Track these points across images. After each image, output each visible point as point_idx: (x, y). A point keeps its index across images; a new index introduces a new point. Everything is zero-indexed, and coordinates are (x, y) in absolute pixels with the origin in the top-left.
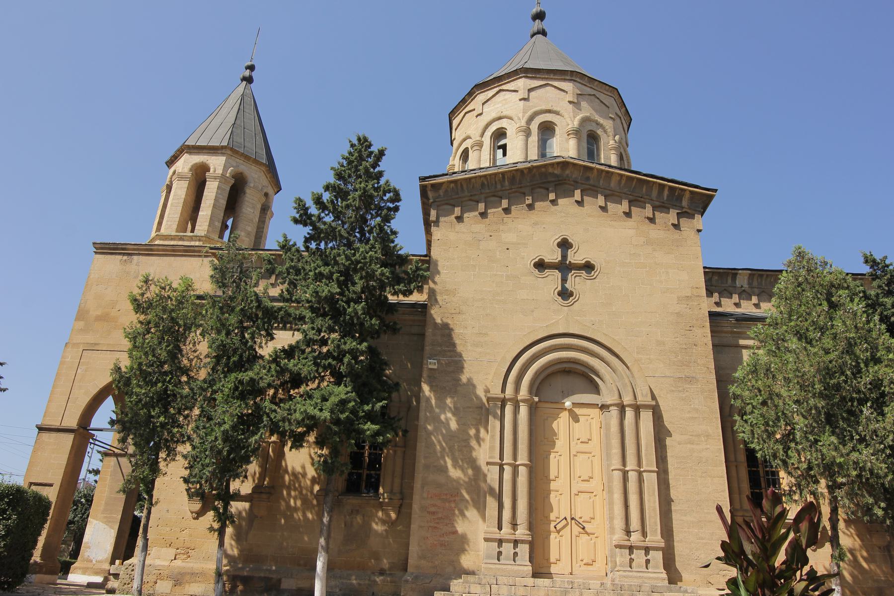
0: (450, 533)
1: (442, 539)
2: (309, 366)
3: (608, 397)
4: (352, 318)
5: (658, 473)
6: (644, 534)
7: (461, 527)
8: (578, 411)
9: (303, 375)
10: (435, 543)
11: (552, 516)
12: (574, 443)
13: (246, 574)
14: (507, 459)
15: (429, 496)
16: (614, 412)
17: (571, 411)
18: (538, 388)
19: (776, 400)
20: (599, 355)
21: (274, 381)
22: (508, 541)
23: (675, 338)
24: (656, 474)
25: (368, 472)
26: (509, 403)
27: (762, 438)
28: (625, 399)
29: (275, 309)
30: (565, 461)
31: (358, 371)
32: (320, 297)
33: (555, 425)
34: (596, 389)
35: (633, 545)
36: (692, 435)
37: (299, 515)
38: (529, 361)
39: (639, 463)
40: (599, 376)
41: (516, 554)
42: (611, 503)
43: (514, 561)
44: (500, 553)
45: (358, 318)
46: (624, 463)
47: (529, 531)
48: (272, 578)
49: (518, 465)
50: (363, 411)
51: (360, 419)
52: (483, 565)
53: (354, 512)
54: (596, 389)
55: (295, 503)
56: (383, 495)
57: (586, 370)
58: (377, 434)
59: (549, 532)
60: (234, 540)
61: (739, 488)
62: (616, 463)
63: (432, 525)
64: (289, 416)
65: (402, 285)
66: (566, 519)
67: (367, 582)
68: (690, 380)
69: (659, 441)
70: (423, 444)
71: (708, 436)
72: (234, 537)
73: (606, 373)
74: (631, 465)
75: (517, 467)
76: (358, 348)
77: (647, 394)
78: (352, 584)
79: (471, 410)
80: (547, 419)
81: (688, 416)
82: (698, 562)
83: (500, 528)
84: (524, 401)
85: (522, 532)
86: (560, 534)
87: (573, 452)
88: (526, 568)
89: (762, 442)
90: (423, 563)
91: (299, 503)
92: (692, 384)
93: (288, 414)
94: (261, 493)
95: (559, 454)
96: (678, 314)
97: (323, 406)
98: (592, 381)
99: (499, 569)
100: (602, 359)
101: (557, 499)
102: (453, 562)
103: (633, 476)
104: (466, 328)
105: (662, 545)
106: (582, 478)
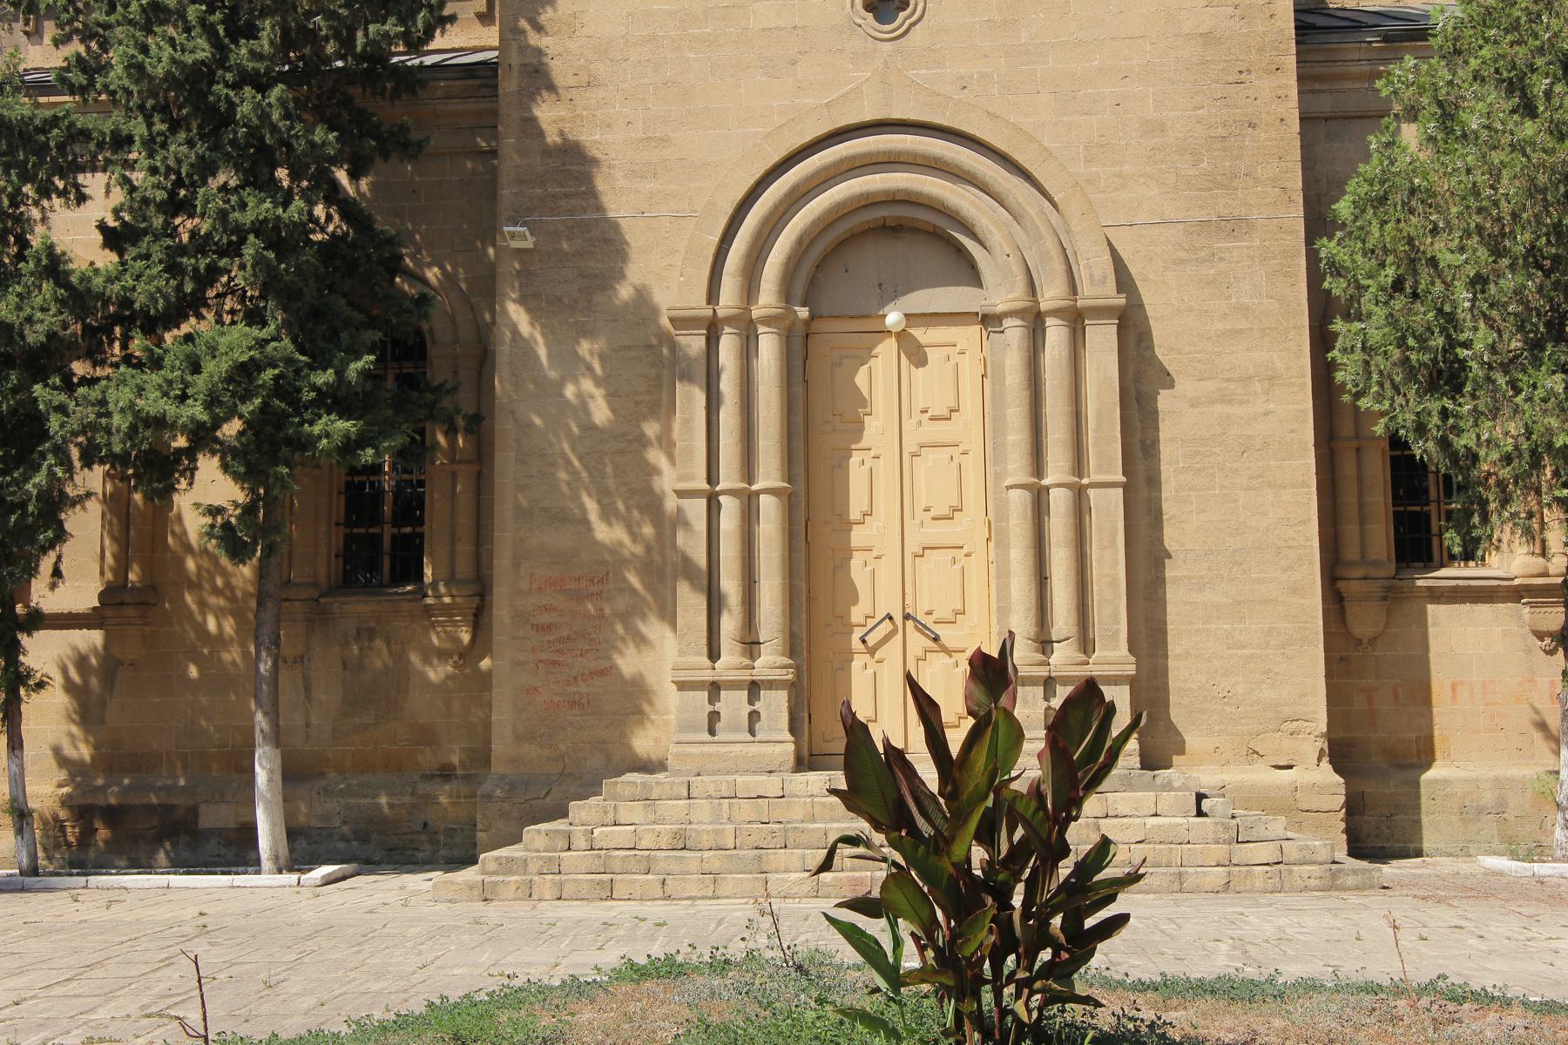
0: (591, 673)
1: (573, 689)
2: (152, 278)
3: (1001, 293)
4: (254, 132)
5: (1127, 488)
6: (1086, 644)
7: (628, 662)
8: (921, 334)
9: (137, 306)
10: (556, 699)
11: (856, 614)
12: (914, 421)
13: (113, 801)
14: (729, 477)
15: (535, 586)
16: (1014, 331)
17: (902, 337)
18: (813, 282)
19: (1425, 273)
20: (974, 176)
21: (65, 326)
22: (734, 685)
23: (1195, 109)
24: (1120, 491)
25: (395, 530)
26: (727, 329)
27: (1392, 381)
28: (1047, 295)
29: (37, 122)
30: (886, 472)
31: (287, 278)
32: (151, 78)
33: (861, 379)
34: (971, 274)
35: (1053, 674)
36: (1229, 380)
37: (232, 655)
38: (782, 210)
39: (1079, 466)
40: (974, 236)
41: (754, 716)
42: (1004, 574)
43: (752, 732)
44: (714, 717)
45: (274, 128)
46: (1038, 466)
47: (791, 657)
48: (174, 806)
49: (758, 493)
50: (314, 388)
51: (306, 409)
52: (673, 749)
53: (366, 634)
54: (971, 274)
55: (220, 626)
56: (434, 585)
57: (941, 222)
58: (349, 446)
59: (848, 656)
60: (74, 721)
61: (1361, 506)
62: (1017, 468)
63: (544, 656)
64: (103, 420)
65: (392, 20)
66: (891, 618)
67: (407, 799)
68: (1233, 226)
69: (1138, 400)
70: (512, 454)
71: (1272, 379)
72: (75, 716)
73: (992, 228)
74: (1057, 470)
75: (753, 499)
76: (278, 218)
77: (1105, 277)
78: (378, 807)
79: (633, 354)
80: (840, 364)
81: (1220, 327)
82: (1226, 704)
83: (714, 654)
84: (768, 321)
85: (771, 661)
86: (877, 656)
87: (910, 446)
88: (778, 748)
89: (1389, 392)
90: (530, 750)
91: (229, 627)
92: (1236, 239)
93: (100, 415)
94: (122, 604)
95: (872, 453)
96: (1208, 38)
97: (187, 385)
98: (960, 250)
99: (710, 755)
100: (984, 188)
101: (869, 568)
102: (604, 742)
103: (1059, 500)
104: (609, 126)
105: (1131, 670)
106: (933, 513)
